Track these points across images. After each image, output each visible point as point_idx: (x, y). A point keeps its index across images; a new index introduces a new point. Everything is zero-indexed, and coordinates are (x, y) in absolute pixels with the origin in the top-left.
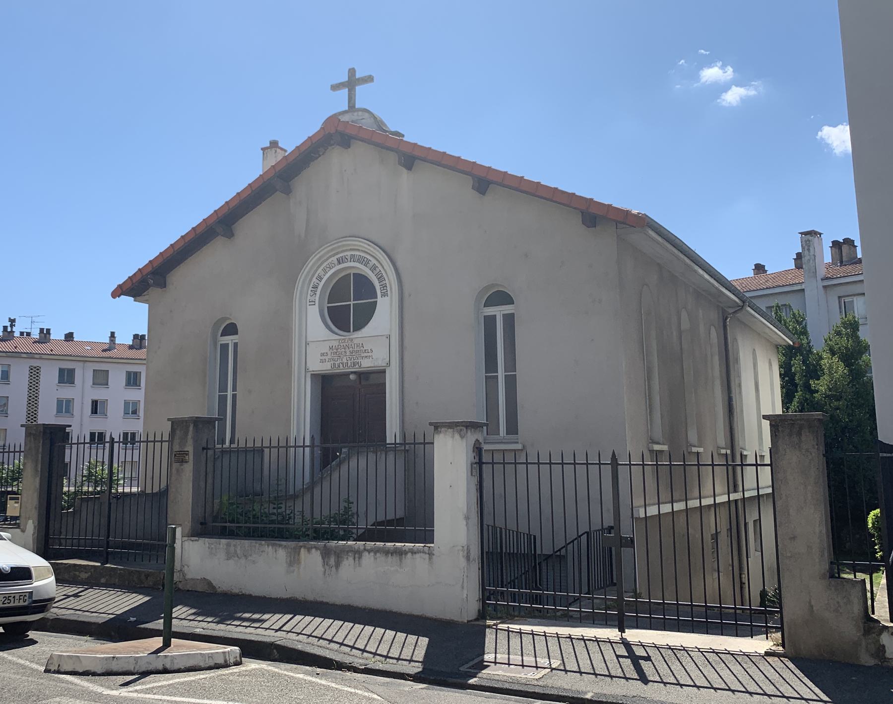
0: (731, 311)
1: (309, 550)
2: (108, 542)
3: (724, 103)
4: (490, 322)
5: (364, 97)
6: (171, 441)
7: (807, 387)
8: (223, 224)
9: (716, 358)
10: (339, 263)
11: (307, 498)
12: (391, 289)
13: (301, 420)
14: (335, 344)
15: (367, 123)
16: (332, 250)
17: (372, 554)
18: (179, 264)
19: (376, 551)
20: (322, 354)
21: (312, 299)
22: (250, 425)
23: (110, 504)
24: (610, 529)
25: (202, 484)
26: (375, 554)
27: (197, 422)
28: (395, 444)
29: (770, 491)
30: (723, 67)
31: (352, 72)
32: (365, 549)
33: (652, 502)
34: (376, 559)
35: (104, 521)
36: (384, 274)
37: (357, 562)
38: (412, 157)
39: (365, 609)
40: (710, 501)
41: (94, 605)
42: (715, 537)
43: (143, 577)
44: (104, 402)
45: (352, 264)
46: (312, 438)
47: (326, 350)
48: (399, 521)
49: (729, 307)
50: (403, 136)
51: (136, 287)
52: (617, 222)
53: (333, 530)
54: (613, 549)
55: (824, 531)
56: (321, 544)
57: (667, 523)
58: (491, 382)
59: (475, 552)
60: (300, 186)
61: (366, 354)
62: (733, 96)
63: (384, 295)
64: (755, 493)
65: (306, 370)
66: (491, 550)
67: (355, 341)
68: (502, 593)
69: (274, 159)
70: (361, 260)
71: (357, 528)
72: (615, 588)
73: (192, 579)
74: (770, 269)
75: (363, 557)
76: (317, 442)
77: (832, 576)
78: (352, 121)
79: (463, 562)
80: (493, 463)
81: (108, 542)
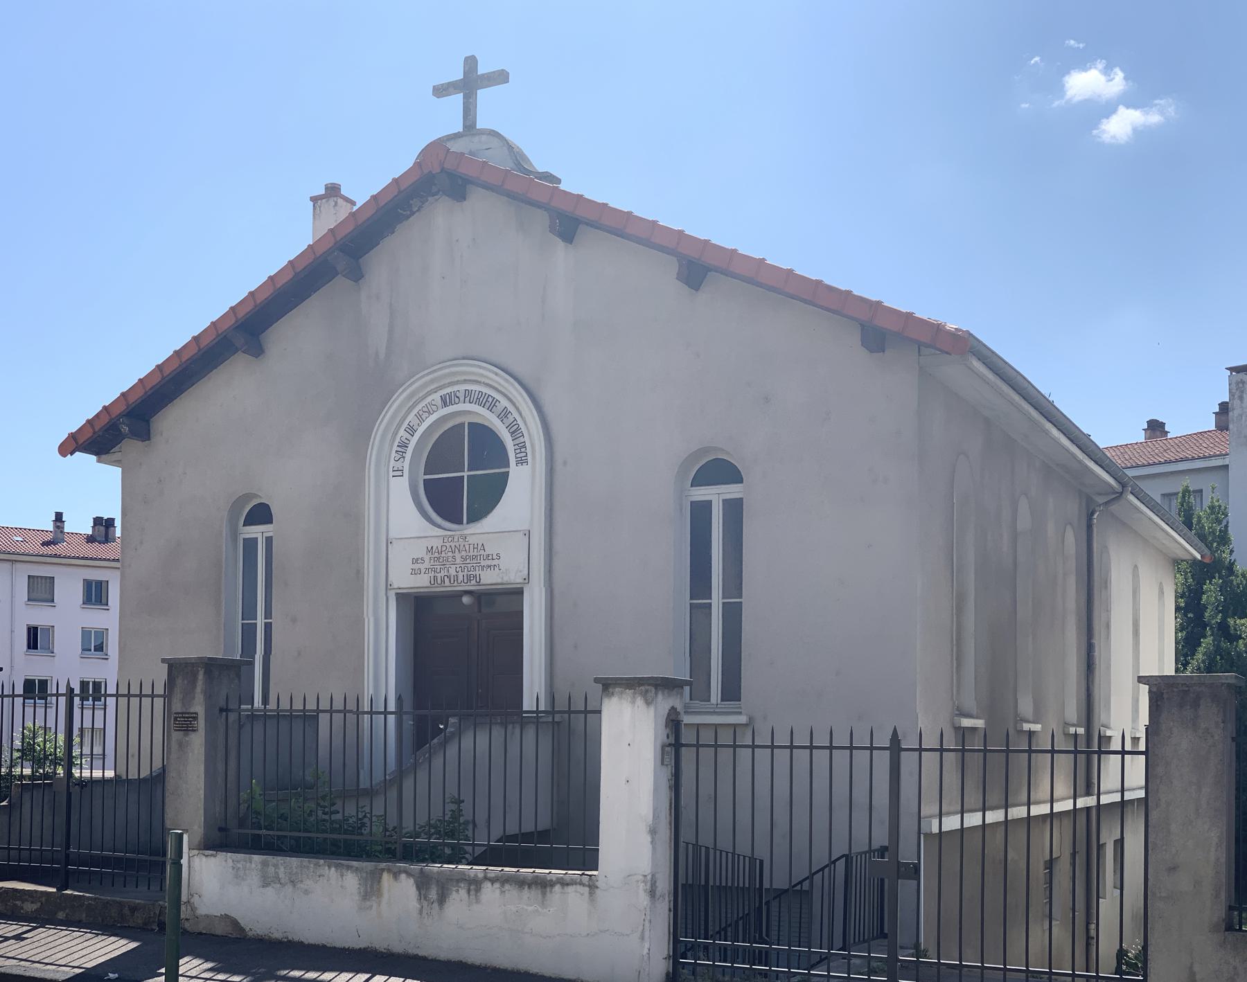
0: (1101, 500)
1: (396, 876)
2: (67, 856)
3: (1106, 138)
4: (701, 512)
5: (493, 109)
6: (168, 696)
7: (1225, 632)
8: (244, 332)
9: (1072, 581)
10: (445, 404)
11: (393, 794)
12: (533, 446)
13: (380, 668)
14: (437, 543)
15: (498, 159)
16: (432, 381)
17: (497, 885)
18: (171, 400)
19: (504, 880)
20: (415, 561)
21: (398, 465)
22: (292, 675)
23: (69, 795)
24: (883, 851)
25: (221, 767)
26: (503, 885)
27: (212, 666)
28: (537, 712)
29: (1142, 794)
30: (1107, 71)
31: (471, 62)
32: (486, 878)
33: (952, 809)
34: (503, 892)
35: (60, 820)
36: (522, 426)
37: (472, 897)
38: (572, 220)
39: (486, 968)
40: (1044, 809)
41: (49, 953)
42: (1050, 864)
43: (126, 911)
44: (49, 630)
45: (468, 407)
46: (399, 699)
47: (421, 553)
48: (543, 836)
49: (1097, 491)
50: (559, 181)
51: (100, 438)
52: (920, 345)
53: (435, 846)
54: (886, 881)
55: (1223, 860)
56: (415, 868)
57: (973, 844)
58: (700, 613)
59: (665, 885)
60: (379, 265)
61: (489, 562)
62: (1120, 125)
63: (521, 461)
64: (1117, 798)
65: (388, 586)
66: (690, 882)
67: (471, 540)
68: (706, 947)
69: (334, 216)
70: (482, 400)
71: (474, 845)
72: (885, 942)
73: (207, 916)
74: (1175, 430)
75: (483, 890)
76: (408, 706)
77: (1229, 928)
78: (471, 153)
79: (643, 900)
80: (698, 746)
81: (67, 856)
